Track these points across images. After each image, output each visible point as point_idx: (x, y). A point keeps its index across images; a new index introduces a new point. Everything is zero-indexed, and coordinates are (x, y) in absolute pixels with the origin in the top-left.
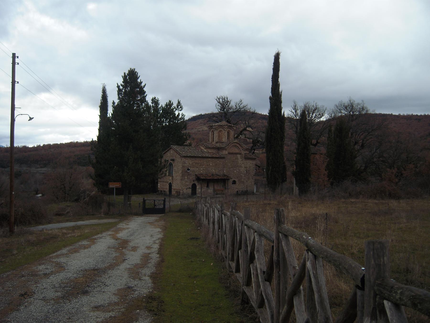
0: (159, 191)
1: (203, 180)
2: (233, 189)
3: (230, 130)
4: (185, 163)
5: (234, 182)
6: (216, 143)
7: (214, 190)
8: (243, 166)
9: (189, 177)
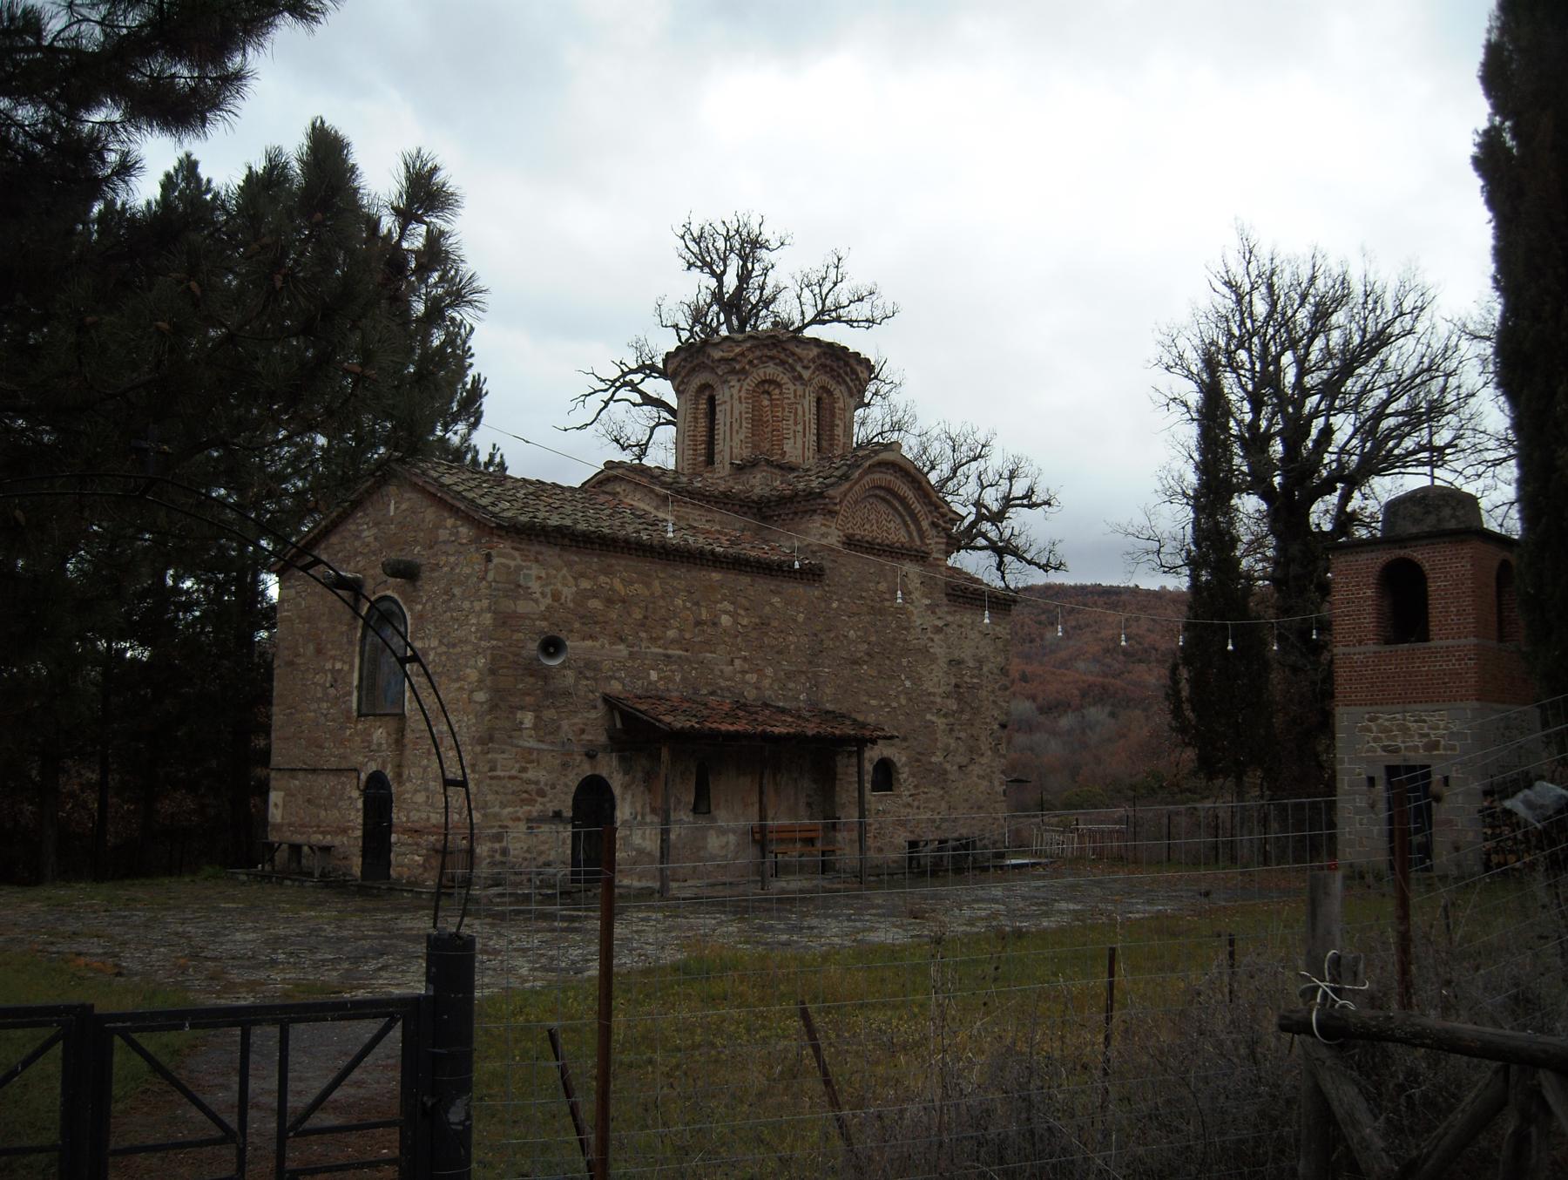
0: (271, 848)
1: (681, 740)
2: (897, 820)
3: (832, 385)
4: (516, 589)
5: (885, 775)
6: (740, 469)
7: (761, 838)
8: (938, 649)
9: (549, 714)
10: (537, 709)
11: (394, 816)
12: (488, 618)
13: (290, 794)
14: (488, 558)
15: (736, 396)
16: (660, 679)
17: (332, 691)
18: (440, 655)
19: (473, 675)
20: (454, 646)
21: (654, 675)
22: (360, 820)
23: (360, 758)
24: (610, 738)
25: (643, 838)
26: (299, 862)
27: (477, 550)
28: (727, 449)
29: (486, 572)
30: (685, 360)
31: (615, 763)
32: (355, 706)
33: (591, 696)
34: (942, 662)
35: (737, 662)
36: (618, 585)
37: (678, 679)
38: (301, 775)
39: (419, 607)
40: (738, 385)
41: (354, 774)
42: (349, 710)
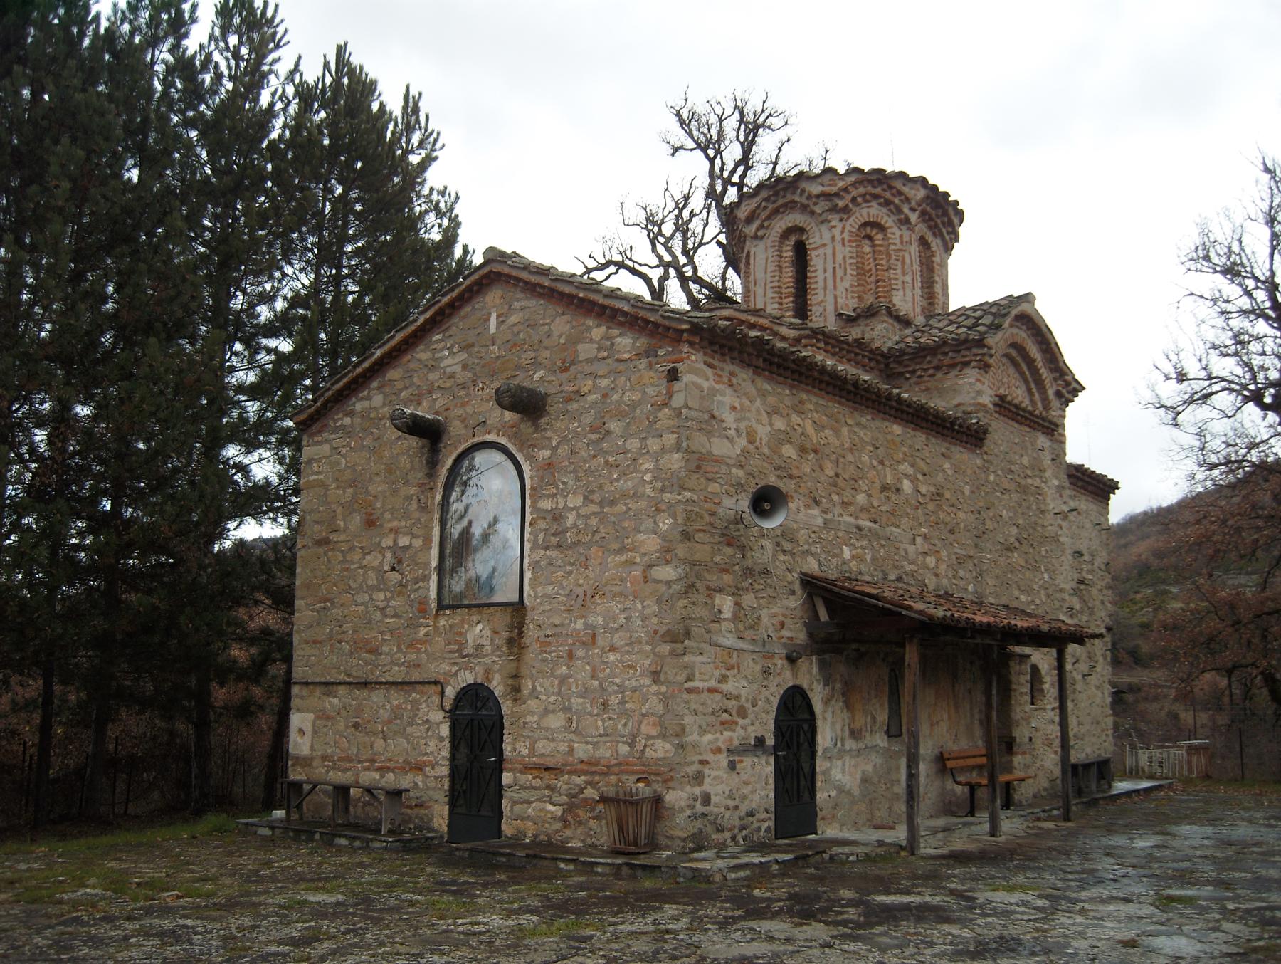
9: (748, 600)
10: (736, 592)
11: (507, 748)
12: (675, 461)
13: (323, 716)
14: (673, 375)
15: (838, 238)
16: (853, 557)
17: (395, 576)
18: (587, 517)
19: (651, 543)
20: (613, 503)
21: (847, 553)
22: (446, 753)
23: (445, 667)
24: (810, 635)
25: (843, 772)
26: (347, 810)
27: (650, 366)
28: (830, 299)
29: (670, 395)
30: (767, 200)
31: (815, 670)
32: (433, 594)
33: (789, 578)
34: (1069, 552)
35: (919, 540)
36: (810, 430)
37: (868, 558)
38: (342, 690)
39: (547, 453)
40: (840, 225)
41: (434, 689)
42: (424, 602)
